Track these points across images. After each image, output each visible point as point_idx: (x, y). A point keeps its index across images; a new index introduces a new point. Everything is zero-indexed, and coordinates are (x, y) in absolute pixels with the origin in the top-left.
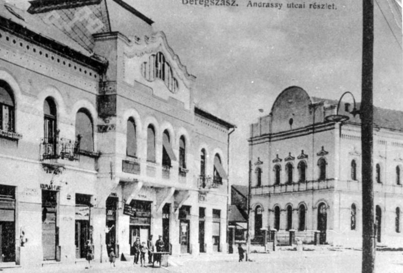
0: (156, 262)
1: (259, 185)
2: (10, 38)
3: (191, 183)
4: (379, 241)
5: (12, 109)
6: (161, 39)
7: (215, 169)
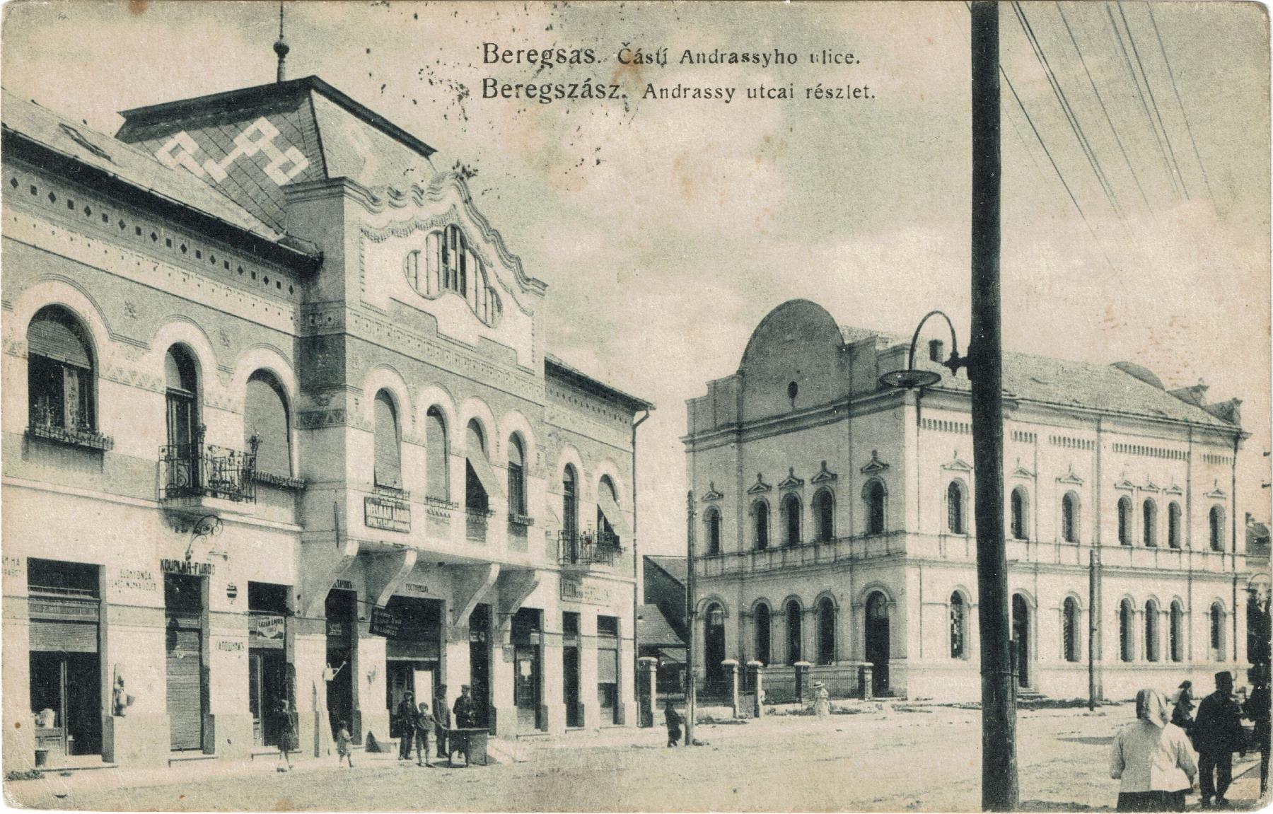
0: (456, 754)
1: (715, 550)
2: (75, 203)
3: (539, 551)
4: (1024, 681)
5: (87, 378)
6: (454, 191)
7: (600, 514)
